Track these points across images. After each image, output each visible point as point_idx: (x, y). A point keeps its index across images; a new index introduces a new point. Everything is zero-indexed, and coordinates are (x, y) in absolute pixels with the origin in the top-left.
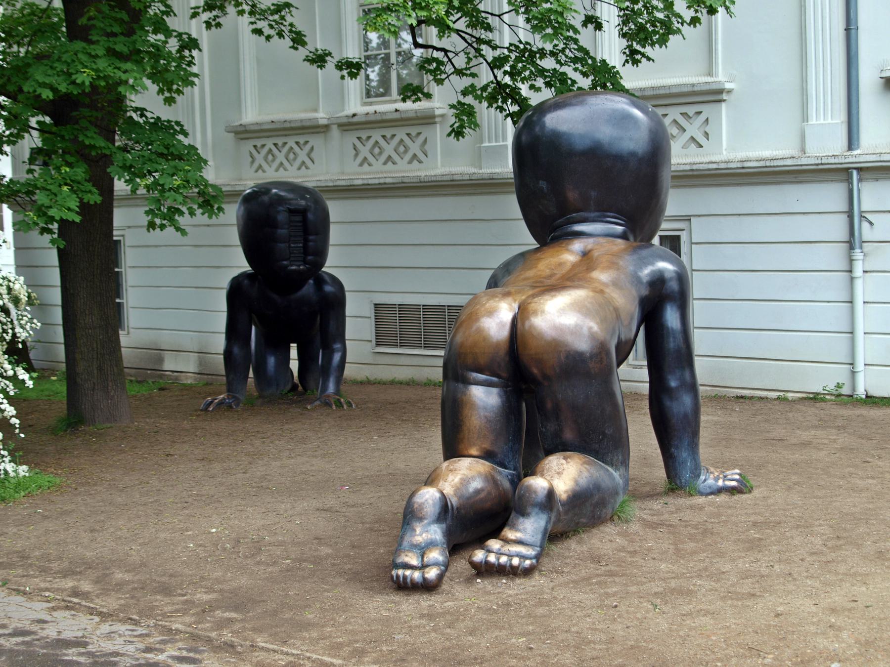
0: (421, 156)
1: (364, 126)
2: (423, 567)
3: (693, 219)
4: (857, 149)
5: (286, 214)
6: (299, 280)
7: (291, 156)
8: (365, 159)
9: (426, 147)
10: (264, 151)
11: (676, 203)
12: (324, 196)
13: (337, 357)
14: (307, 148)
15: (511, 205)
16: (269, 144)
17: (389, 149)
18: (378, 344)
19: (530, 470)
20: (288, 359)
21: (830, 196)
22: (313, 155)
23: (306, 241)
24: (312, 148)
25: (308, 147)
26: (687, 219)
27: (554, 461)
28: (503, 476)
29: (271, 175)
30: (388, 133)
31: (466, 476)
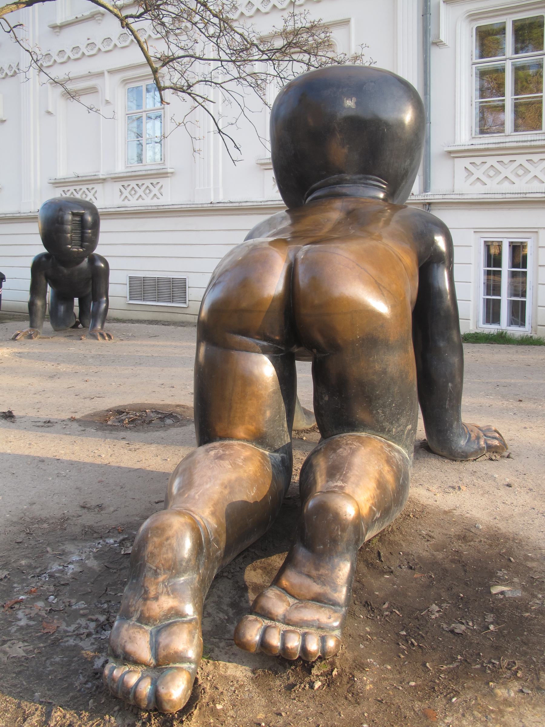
0: (159, 195)
1: (155, 176)
3: (541, 232)
4: (429, 192)
7: (133, 192)
9: (162, 190)
10: (129, 189)
13: (104, 306)
14: (159, 186)
22: (96, 195)
24: (96, 192)
30: (140, 182)
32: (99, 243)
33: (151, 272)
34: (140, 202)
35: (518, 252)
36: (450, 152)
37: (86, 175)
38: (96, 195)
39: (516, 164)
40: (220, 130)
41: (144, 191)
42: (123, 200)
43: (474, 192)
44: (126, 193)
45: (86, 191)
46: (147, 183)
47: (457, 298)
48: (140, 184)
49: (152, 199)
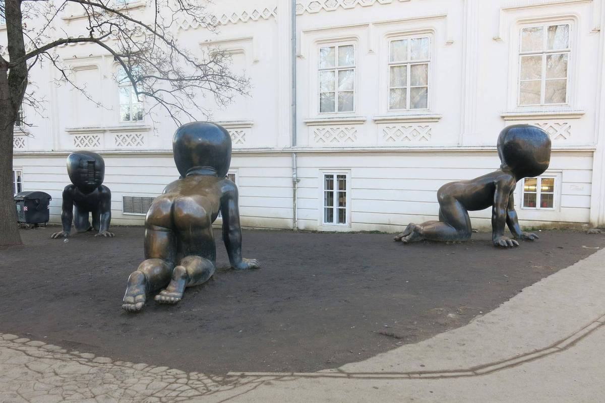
2: (135, 303)
3: (352, 169)
5: (87, 163)
6: (92, 188)
8: (87, 144)
10: (88, 139)
11: (234, 162)
12: (102, 156)
14: (141, 137)
15: (171, 162)
16: (82, 136)
17: (86, 141)
18: (124, 212)
19: (177, 263)
20: (88, 217)
21: (286, 161)
23: (95, 173)
24: (143, 137)
25: (141, 137)
26: (237, 168)
27: (189, 258)
28: (169, 265)
29: (82, 148)
30: (129, 134)
31: (148, 267)
32: (231, 166)
33: (139, 194)
34: (129, 147)
35: (342, 180)
36: (307, 123)
37: (92, 127)
38: (99, 141)
39: (412, 129)
40: (172, 116)
41: (132, 140)
42: (118, 145)
43: (317, 146)
44: (119, 140)
45: (136, 137)
46: (133, 134)
47: (240, 215)
48: (119, 135)
49: (127, 145)
